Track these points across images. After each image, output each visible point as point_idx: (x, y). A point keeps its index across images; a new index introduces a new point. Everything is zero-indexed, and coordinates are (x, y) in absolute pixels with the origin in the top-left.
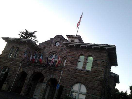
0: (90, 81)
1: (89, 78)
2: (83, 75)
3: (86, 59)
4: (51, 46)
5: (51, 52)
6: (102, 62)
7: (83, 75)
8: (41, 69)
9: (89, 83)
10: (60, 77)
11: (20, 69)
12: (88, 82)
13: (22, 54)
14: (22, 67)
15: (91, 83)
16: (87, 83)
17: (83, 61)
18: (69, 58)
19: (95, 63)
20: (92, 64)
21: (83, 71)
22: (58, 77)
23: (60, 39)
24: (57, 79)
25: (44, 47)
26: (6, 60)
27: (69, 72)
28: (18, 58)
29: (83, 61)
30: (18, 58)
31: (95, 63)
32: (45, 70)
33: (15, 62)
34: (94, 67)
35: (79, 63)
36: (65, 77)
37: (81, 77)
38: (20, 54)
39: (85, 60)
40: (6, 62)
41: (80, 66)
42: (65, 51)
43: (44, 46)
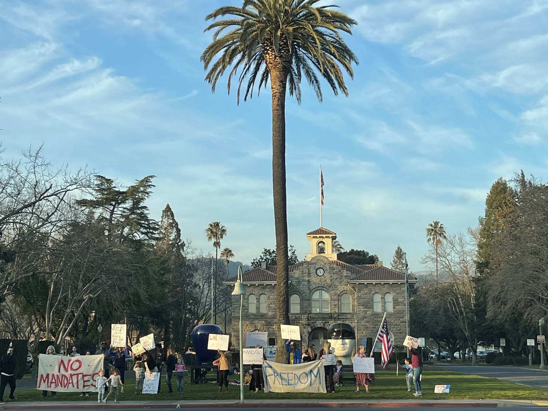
8: (322, 322)
27: (365, 319)
34: (396, 307)
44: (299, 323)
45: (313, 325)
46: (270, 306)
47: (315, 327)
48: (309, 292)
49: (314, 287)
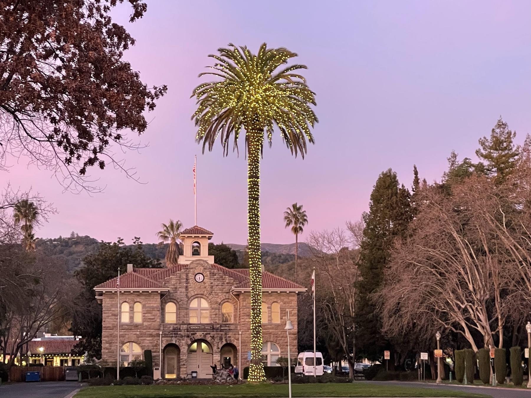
0: (282, 337)
1: (280, 333)
2: (271, 331)
3: (132, 309)
4: (189, 284)
5: (177, 301)
6: (292, 309)
7: (271, 331)
9: (281, 340)
10: (238, 339)
11: (162, 340)
12: (280, 338)
13: (153, 314)
14: (163, 337)
15: (283, 339)
16: (279, 340)
17: (141, 311)
18: (245, 309)
19: (284, 312)
20: (175, 314)
21: (270, 326)
22: (236, 340)
23: (202, 268)
24: (235, 343)
25: (173, 287)
26: (122, 331)
28: (149, 323)
29: (141, 311)
30: (149, 323)
31: (284, 312)
32: (209, 334)
33: (144, 331)
34: (284, 318)
35: (123, 314)
36: (247, 339)
37: (270, 334)
38: (149, 315)
39: (270, 309)
40: (126, 334)
41: (125, 319)
42: (221, 292)
43: (174, 285)
44: (177, 334)
45: (193, 337)
46: (146, 315)
47: (194, 339)
48: (187, 299)
49: (193, 295)
